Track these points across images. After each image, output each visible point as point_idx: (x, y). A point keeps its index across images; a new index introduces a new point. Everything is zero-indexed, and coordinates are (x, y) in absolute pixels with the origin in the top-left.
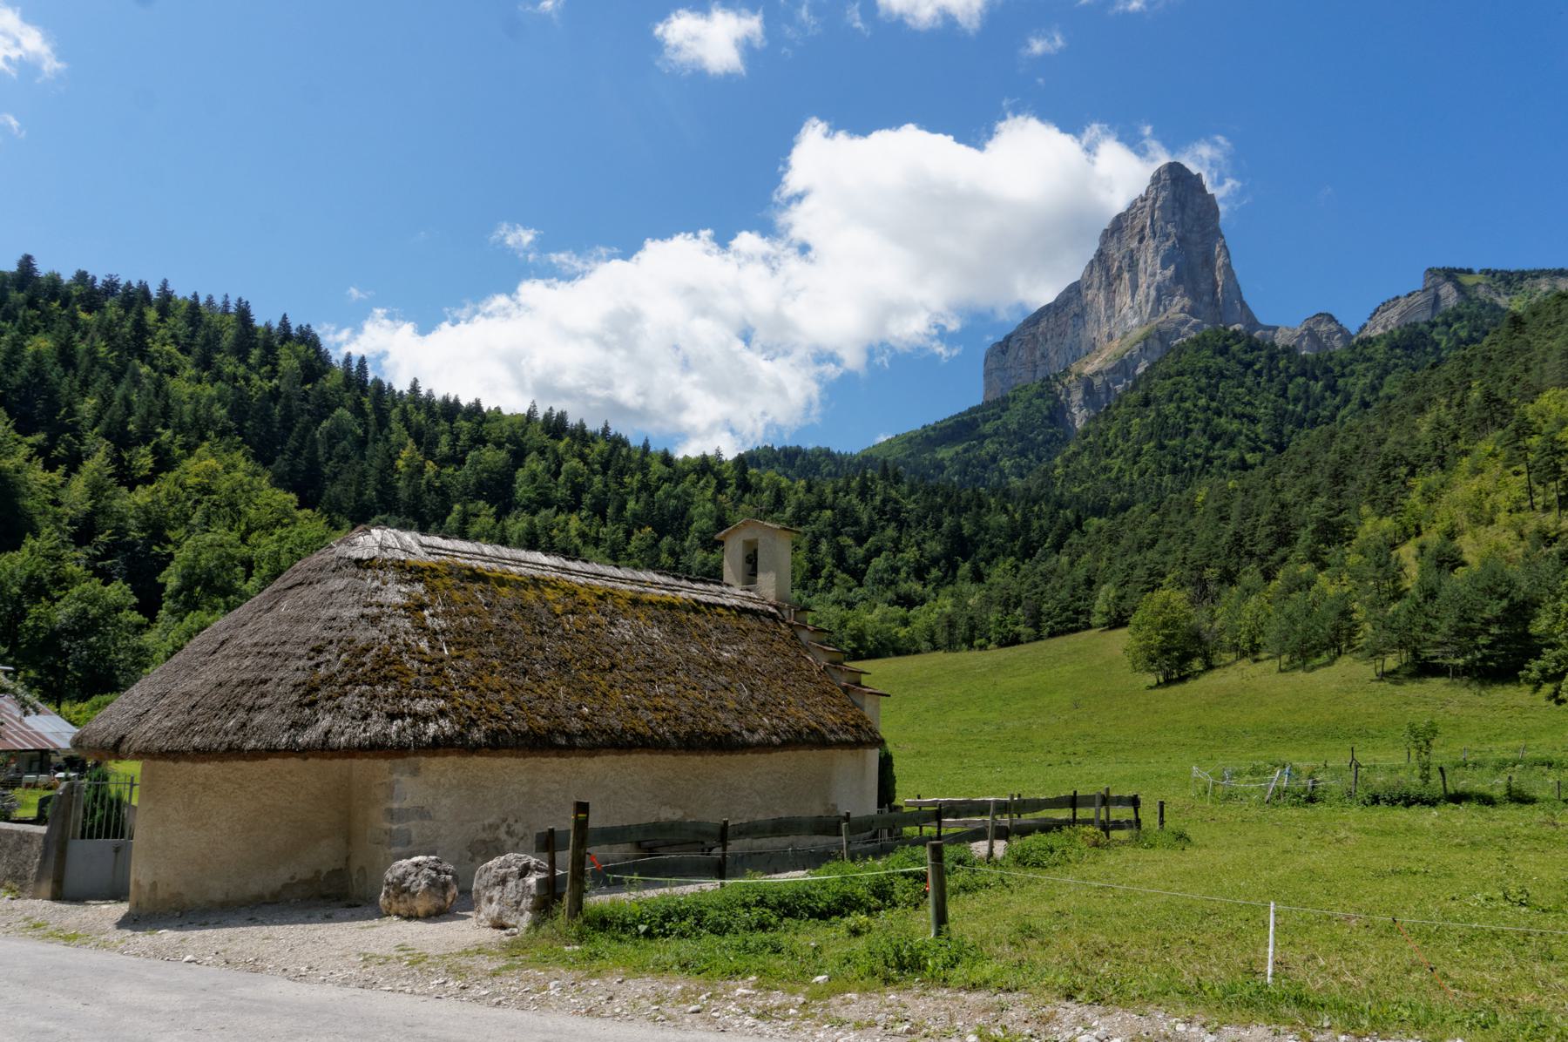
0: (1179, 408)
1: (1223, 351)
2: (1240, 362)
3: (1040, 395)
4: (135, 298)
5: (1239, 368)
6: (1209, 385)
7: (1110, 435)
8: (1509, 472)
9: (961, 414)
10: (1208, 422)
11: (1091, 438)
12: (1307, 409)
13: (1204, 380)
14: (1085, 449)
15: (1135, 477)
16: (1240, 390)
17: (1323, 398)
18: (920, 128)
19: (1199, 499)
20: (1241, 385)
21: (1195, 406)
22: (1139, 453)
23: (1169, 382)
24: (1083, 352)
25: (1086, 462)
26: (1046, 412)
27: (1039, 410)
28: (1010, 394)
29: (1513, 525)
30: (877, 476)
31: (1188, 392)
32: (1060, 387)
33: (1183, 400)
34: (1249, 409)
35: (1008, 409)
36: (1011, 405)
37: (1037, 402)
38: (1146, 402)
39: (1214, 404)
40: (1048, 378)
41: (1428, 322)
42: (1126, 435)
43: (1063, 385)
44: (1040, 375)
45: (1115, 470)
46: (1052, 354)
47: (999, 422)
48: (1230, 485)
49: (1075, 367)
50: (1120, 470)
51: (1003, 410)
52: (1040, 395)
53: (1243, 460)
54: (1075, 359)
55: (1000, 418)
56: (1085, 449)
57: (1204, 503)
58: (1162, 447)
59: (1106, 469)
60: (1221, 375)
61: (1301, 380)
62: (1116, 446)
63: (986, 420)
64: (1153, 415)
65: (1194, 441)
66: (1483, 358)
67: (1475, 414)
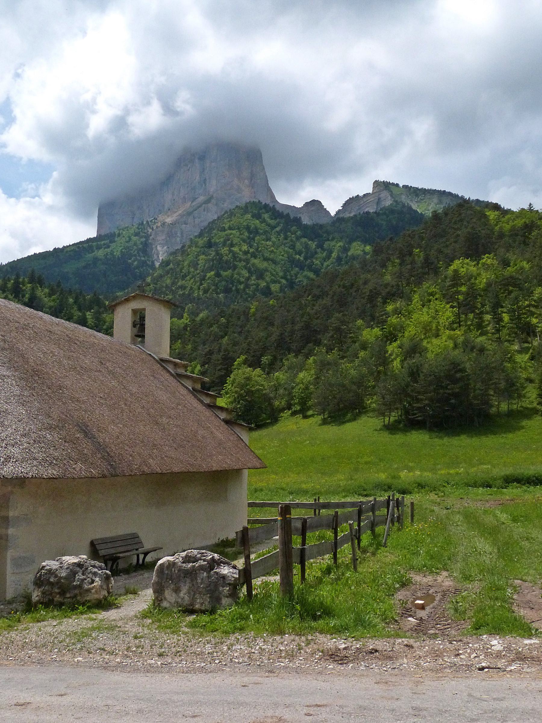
0: (230, 251)
1: (257, 216)
2: (269, 225)
3: (136, 234)
4: (170, 336)
5: (267, 229)
6: (249, 238)
7: (186, 263)
8: (448, 306)
9: (81, 243)
10: (247, 261)
11: (171, 266)
12: (306, 258)
13: (246, 234)
14: (168, 272)
15: (201, 293)
16: (268, 243)
17: (316, 253)
18: (14, 261)
19: (252, 310)
20: (268, 239)
21: (240, 250)
22: (203, 279)
23: (224, 233)
24: (166, 207)
25: (168, 281)
26: (141, 246)
27: (135, 244)
28: (117, 232)
29: (450, 337)
30: (26, 280)
31: (236, 241)
32: (150, 230)
33: (232, 245)
34: (272, 256)
35: (115, 242)
36: (116, 239)
37: (134, 238)
38: (210, 245)
39: (251, 250)
40: (142, 223)
41: (376, 213)
42: (195, 265)
43: (153, 229)
44: (137, 221)
45: (188, 288)
46: (145, 207)
47: (108, 250)
48: (271, 302)
49: (161, 218)
50: (191, 288)
51: (111, 242)
52: (136, 234)
53: (268, 288)
54: (160, 212)
55: (108, 247)
56: (168, 272)
57: (254, 315)
58: (218, 275)
59: (183, 287)
60: (256, 232)
61: (304, 240)
62: (189, 273)
63: (99, 248)
64: (214, 253)
65: (239, 274)
66: (419, 237)
67: (420, 270)
